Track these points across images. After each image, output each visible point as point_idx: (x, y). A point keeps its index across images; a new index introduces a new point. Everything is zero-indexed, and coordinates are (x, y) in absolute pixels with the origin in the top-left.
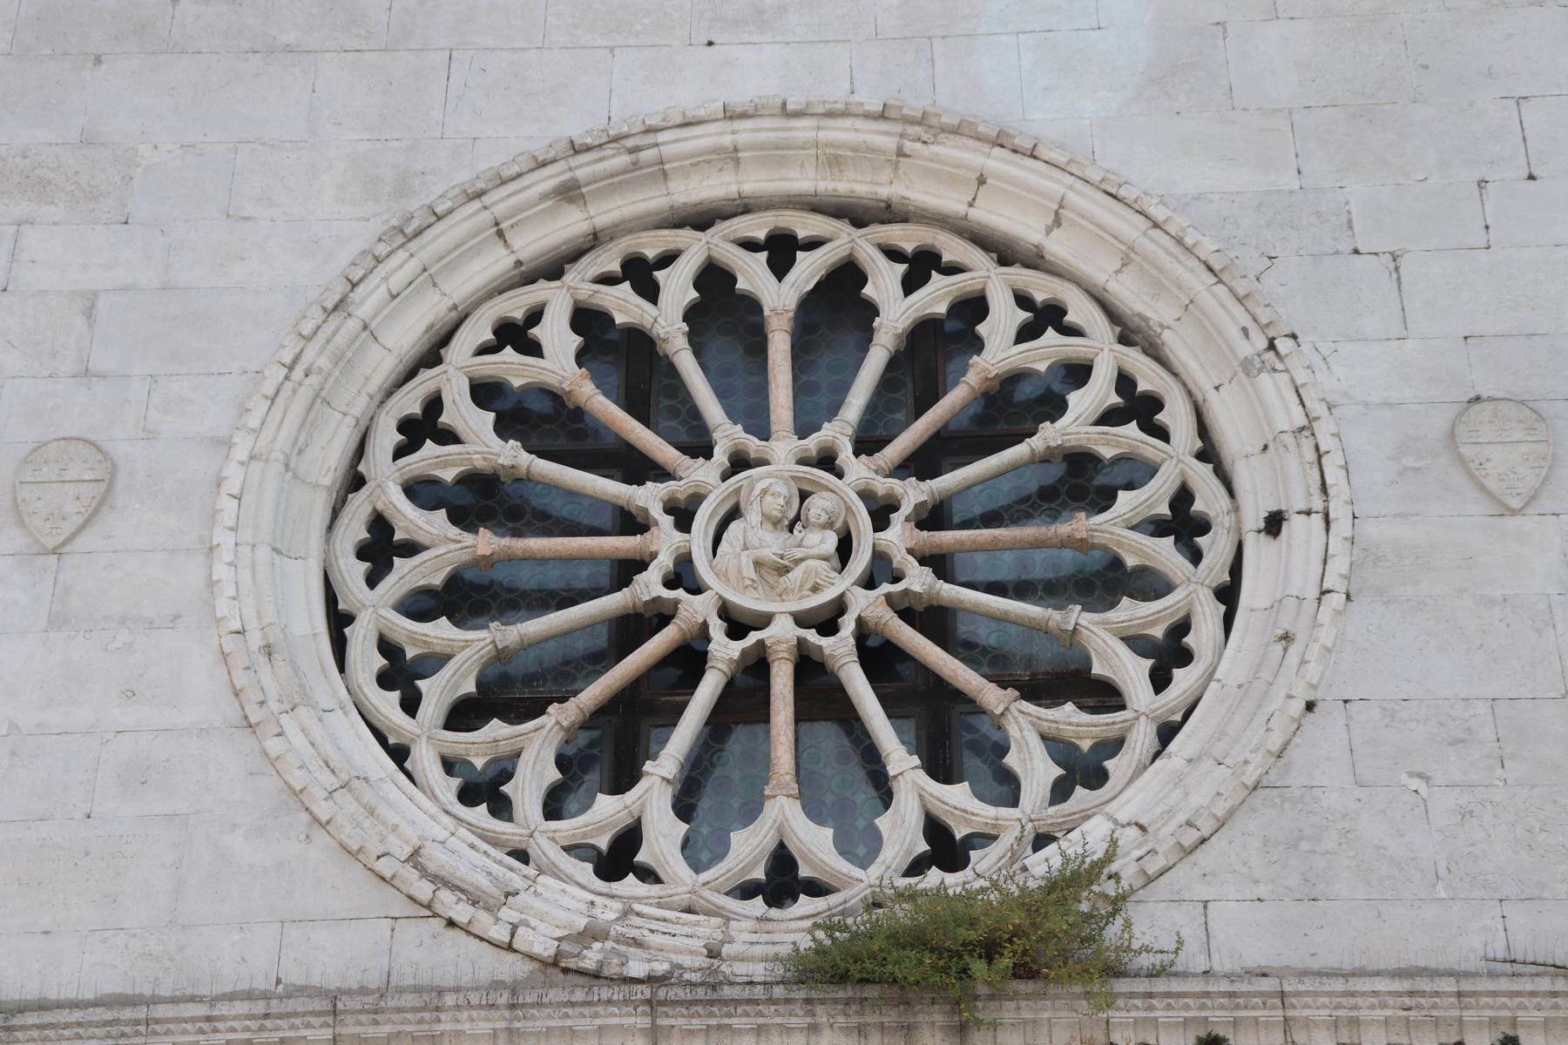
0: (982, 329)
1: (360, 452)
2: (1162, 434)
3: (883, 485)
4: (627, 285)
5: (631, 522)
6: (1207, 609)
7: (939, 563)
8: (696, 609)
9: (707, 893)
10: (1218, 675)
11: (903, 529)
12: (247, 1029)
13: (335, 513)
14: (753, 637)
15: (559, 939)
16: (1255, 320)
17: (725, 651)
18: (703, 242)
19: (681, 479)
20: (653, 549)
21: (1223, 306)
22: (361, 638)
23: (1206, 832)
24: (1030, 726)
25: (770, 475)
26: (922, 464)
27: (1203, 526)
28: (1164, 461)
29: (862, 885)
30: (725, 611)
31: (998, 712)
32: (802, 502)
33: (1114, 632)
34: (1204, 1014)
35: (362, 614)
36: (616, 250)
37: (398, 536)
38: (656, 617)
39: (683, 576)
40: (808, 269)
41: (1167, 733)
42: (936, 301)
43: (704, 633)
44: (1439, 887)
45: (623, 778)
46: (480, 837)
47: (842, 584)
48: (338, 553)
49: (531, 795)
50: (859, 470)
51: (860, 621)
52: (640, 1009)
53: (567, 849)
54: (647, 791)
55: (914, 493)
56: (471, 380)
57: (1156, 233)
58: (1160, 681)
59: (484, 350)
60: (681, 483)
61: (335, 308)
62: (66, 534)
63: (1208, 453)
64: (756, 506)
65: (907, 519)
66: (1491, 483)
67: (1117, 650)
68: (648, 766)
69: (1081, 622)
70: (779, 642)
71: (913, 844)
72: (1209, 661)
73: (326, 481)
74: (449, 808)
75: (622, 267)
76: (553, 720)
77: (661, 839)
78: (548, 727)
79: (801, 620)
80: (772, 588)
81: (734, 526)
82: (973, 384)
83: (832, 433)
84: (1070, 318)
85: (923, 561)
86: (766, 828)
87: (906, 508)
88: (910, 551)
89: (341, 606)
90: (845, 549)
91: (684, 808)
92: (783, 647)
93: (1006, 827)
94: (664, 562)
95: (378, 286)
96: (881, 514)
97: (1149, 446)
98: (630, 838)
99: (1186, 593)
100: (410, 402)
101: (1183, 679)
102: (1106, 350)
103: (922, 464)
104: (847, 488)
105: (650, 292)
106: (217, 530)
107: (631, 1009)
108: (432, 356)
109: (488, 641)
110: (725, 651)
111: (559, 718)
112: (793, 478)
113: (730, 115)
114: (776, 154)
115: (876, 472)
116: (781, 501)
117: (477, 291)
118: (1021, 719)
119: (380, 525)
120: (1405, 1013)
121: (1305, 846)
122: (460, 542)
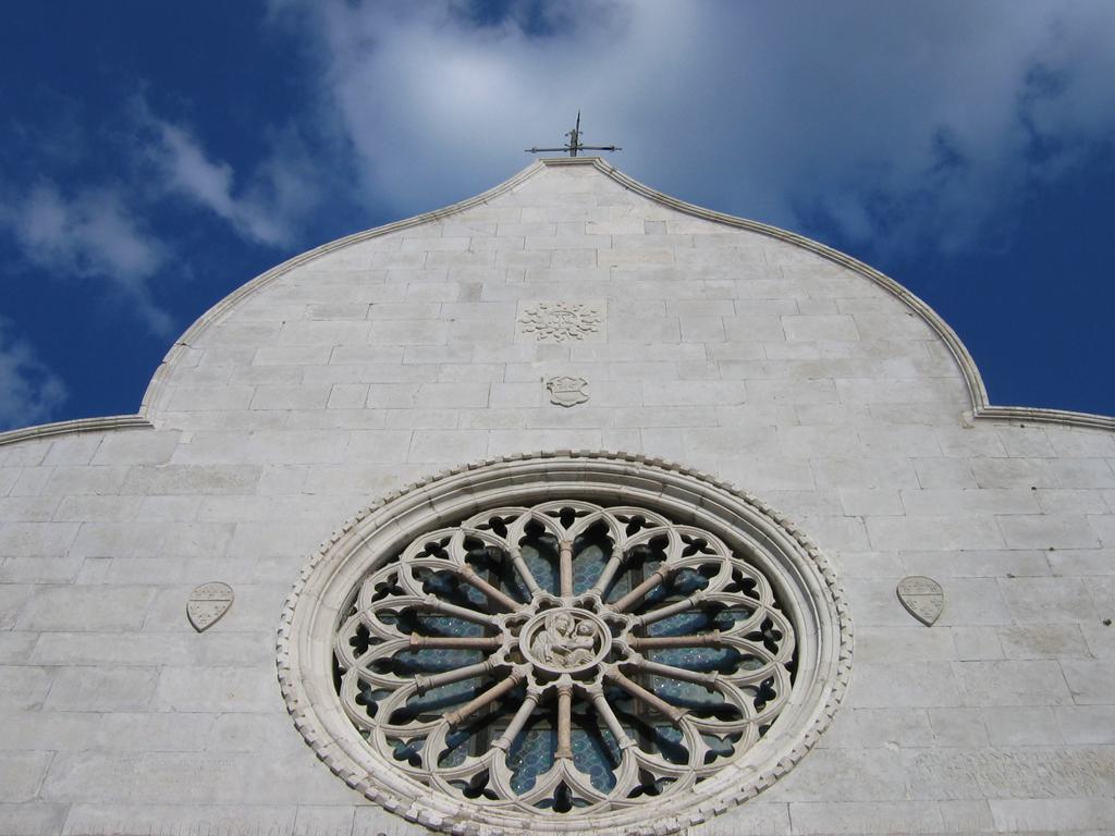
0: (666, 551)
1: (355, 599)
2: (756, 596)
3: (617, 617)
8: (521, 670)
13: (341, 624)
14: (550, 684)
17: (535, 689)
23: (787, 769)
26: (639, 607)
27: (778, 636)
33: (735, 684)
37: (371, 635)
38: (501, 673)
40: (580, 525)
41: (763, 730)
43: (524, 682)
45: (481, 749)
46: (410, 776)
47: (596, 660)
50: (605, 610)
51: (605, 677)
53: (450, 783)
55: (633, 620)
59: (419, 556)
66: (918, 612)
71: (632, 781)
73: (337, 607)
79: (575, 676)
81: (542, 634)
84: (709, 546)
85: (637, 651)
87: (629, 627)
88: (630, 646)
89: (340, 666)
90: (597, 647)
92: (566, 689)
94: (506, 648)
96: (617, 628)
97: (750, 601)
100: (382, 576)
103: (639, 607)
105: (503, 533)
110: (535, 689)
111: (450, 717)
113: (545, 456)
119: (363, 631)
121: (838, 776)
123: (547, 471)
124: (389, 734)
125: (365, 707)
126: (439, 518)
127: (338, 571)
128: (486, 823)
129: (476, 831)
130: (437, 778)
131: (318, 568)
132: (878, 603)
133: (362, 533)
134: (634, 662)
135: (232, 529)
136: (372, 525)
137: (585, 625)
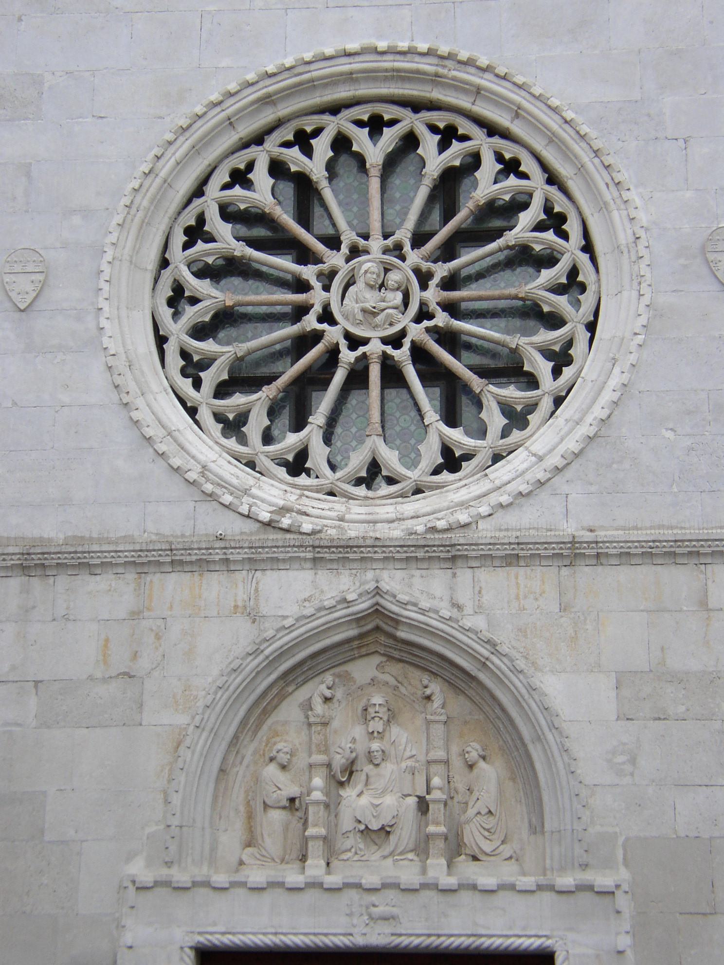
3: (425, 266)
4: (297, 148)
5: (302, 286)
6: (581, 337)
7: (451, 308)
8: (333, 334)
9: (339, 484)
10: (582, 375)
11: (435, 291)
12: (133, 556)
13: (156, 280)
14: (361, 350)
15: (270, 512)
16: (612, 179)
18: (336, 123)
19: (324, 263)
20: (312, 302)
21: (597, 170)
22: (172, 351)
24: (492, 399)
25: (369, 261)
28: (565, 252)
29: (411, 480)
30: (348, 336)
31: (477, 392)
32: (385, 275)
33: (535, 348)
34: (561, 552)
35: (172, 337)
36: (290, 128)
39: (327, 317)
41: (558, 401)
42: (455, 158)
44: (674, 486)
45: (299, 424)
48: (159, 304)
49: (256, 434)
50: (414, 257)
52: (308, 549)
54: (310, 432)
55: (441, 270)
56: (219, 204)
57: (566, 127)
58: (557, 372)
60: (325, 265)
61: (150, 172)
62: (29, 301)
63: (588, 248)
64: (362, 279)
65: (437, 286)
67: (537, 359)
68: (310, 419)
69: (520, 343)
70: (373, 354)
71: (436, 459)
72: (580, 363)
74: (218, 440)
75: (294, 136)
76: (265, 395)
77: (317, 457)
78: (263, 399)
79: (385, 341)
80: (370, 324)
81: (352, 289)
82: (471, 208)
83: (400, 237)
86: (366, 452)
87: (436, 280)
90: (406, 302)
91: (328, 439)
93: (479, 451)
94: (318, 309)
95: (170, 158)
96: (424, 279)
98: (302, 455)
99: (570, 328)
101: (568, 372)
102: (539, 189)
104: (407, 267)
105: (308, 151)
106: (101, 299)
107: (304, 549)
108: (199, 192)
109: (233, 352)
110: (347, 356)
111: (268, 392)
112: (381, 262)
114: (371, 75)
115: (422, 259)
116: (375, 276)
117: (220, 156)
118: (488, 395)
120: (650, 550)
121: (615, 466)
122: (217, 298)
123: (351, 73)
124: (214, 410)
125: (190, 380)
126: (241, 139)
127: (145, 224)
128: (308, 515)
129: (300, 526)
130: (263, 458)
131: (127, 226)
132: (682, 261)
133: (163, 174)
134: (441, 324)
135: (26, 170)
136: (172, 161)
137: (394, 277)
